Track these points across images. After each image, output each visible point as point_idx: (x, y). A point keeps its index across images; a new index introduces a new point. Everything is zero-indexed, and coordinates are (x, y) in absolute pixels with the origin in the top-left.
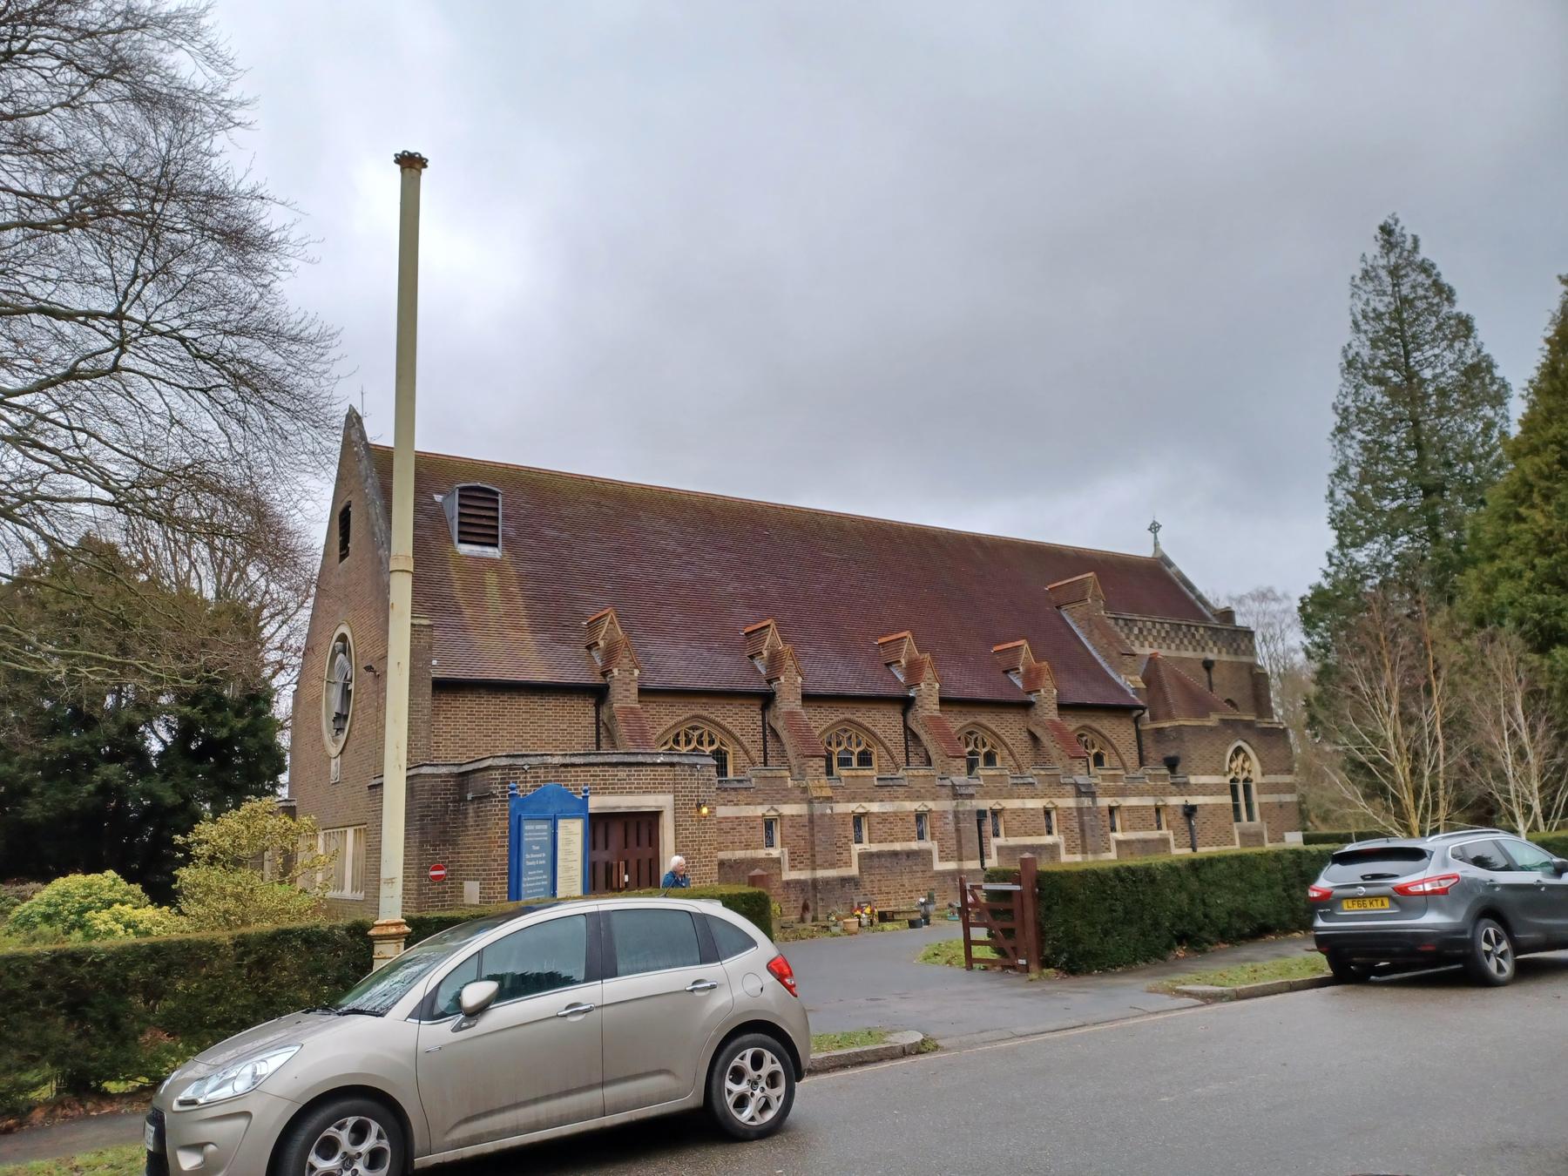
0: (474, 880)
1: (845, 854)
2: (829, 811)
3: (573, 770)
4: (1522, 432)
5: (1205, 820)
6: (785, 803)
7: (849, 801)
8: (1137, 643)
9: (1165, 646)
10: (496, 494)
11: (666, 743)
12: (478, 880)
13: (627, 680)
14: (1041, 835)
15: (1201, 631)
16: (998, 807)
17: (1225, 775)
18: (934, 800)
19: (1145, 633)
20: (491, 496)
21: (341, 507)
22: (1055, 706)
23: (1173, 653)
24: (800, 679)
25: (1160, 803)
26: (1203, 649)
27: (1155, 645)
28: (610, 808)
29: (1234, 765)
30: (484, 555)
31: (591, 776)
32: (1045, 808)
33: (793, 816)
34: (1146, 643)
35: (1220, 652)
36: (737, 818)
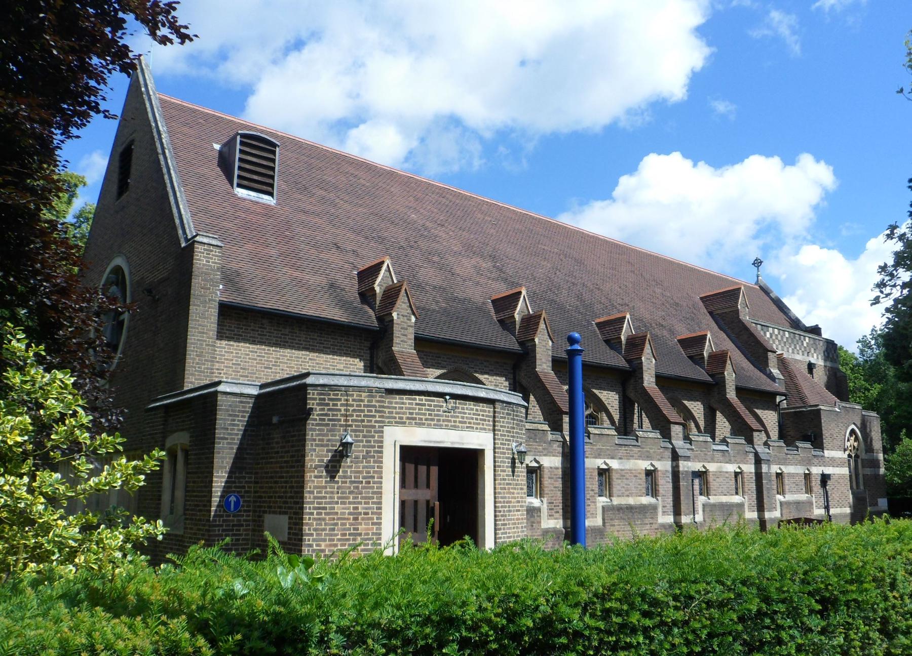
0: (280, 513)
3: (417, 397)
4: (191, 437)
5: (833, 487)
6: (545, 455)
10: (275, 145)
12: (285, 513)
15: (807, 339)
16: (605, 467)
17: (845, 450)
18: (659, 460)
21: (120, 149)
22: (734, 387)
24: (550, 343)
25: (807, 472)
28: (435, 442)
30: (260, 201)
31: (417, 404)
33: (551, 468)
35: (818, 358)
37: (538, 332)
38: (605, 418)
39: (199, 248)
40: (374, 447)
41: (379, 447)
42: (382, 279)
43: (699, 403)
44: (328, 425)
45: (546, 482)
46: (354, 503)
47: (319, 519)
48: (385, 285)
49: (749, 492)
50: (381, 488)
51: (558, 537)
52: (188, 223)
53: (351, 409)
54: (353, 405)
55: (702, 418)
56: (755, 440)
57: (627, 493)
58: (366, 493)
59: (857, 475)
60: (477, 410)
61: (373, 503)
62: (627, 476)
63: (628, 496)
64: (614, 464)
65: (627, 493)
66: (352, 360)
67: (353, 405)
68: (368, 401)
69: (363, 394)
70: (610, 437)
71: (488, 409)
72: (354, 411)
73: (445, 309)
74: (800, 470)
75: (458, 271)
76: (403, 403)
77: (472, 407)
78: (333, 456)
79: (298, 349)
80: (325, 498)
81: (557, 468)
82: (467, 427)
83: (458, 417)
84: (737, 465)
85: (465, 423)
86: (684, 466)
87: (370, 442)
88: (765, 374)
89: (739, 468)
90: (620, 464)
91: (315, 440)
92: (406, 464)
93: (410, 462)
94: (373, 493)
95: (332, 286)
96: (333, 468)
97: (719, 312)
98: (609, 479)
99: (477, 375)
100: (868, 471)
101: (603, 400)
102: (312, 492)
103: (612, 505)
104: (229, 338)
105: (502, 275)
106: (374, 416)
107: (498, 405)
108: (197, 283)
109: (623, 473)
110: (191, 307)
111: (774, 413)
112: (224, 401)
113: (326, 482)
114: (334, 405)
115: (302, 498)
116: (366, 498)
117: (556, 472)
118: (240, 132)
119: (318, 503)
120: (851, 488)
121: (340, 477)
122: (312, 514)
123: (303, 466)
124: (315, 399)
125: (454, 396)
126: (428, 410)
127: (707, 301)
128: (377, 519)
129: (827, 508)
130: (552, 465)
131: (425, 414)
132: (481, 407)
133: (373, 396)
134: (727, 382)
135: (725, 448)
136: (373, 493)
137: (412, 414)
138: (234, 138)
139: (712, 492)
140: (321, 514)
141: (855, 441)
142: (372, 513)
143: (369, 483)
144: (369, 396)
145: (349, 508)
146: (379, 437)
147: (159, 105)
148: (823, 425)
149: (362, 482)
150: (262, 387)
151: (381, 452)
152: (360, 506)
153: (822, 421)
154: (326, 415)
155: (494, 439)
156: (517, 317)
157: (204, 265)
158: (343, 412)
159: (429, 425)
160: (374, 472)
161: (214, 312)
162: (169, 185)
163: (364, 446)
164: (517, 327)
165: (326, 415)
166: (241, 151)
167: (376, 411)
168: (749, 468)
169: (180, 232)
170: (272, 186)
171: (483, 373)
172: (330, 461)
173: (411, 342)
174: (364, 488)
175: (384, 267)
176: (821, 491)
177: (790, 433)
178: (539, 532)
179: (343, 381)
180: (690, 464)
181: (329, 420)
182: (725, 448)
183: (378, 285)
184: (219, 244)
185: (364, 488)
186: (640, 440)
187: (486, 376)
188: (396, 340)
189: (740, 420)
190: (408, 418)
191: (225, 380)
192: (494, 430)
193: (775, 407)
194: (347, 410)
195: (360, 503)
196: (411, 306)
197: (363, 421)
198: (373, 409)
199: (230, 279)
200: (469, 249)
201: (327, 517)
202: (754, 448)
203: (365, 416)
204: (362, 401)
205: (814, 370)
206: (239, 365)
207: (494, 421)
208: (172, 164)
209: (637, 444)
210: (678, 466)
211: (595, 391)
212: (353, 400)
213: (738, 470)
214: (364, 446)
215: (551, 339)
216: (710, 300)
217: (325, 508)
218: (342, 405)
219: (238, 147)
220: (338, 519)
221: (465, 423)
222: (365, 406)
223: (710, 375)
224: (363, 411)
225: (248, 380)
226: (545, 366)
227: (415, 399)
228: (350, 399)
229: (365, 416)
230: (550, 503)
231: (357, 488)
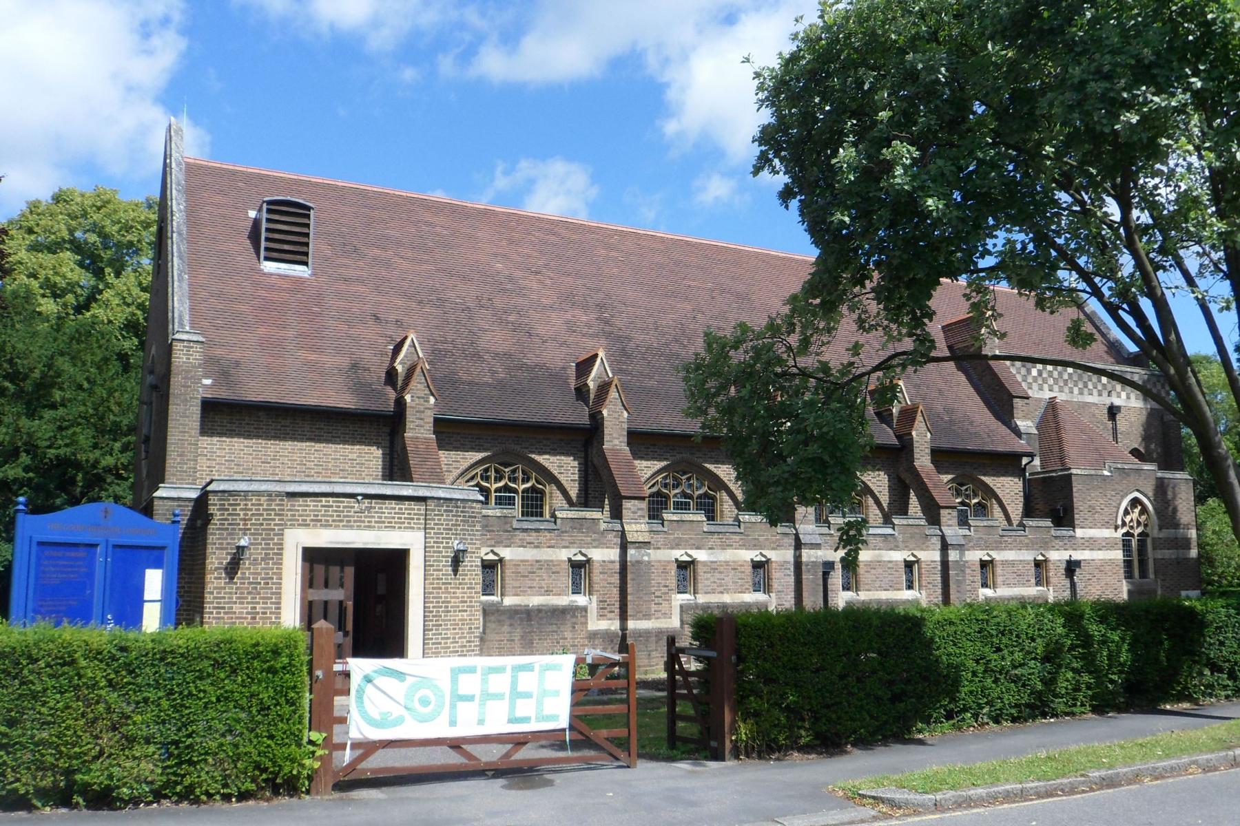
1: (665, 604)
2: (646, 558)
3: (324, 499)
5: (1088, 576)
6: (595, 547)
7: (673, 548)
8: (1035, 386)
9: (1066, 389)
10: (309, 208)
11: (472, 478)
13: (422, 408)
14: (899, 590)
16: (686, 558)
17: (1116, 528)
18: (773, 549)
19: (1045, 375)
20: (302, 210)
22: (928, 451)
23: (1076, 398)
24: (626, 414)
25: (1040, 558)
26: (1109, 394)
27: (1056, 388)
28: (343, 543)
29: (1128, 519)
30: (292, 273)
31: (322, 506)
32: (905, 561)
33: (604, 561)
34: (1046, 386)
35: (1128, 398)
36: (537, 561)
37: (607, 402)
38: (725, 497)
39: (177, 346)
40: (273, 549)
41: (278, 549)
42: (405, 356)
43: (882, 473)
44: (227, 529)
45: (597, 577)
46: (252, 603)
47: (219, 618)
48: (409, 363)
49: (930, 586)
50: (280, 588)
51: (612, 641)
52: (181, 317)
53: (250, 513)
54: (251, 510)
55: (886, 492)
56: (943, 520)
57: (721, 589)
58: (264, 593)
59: (1143, 563)
60: (401, 509)
61: (271, 603)
62: (722, 569)
63: (722, 593)
64: (701, 555)
65: (721, 589)
66: (366, 448)
67: (251, 510)
68: (268, 505)
69: (262, 498)
70: (695, 525)
71: (419, 508)
72: (253, 515)
73: (500, 381)
74: (1029, 556)
75: (540, 330)
76: (307, 506)
77: (393, 506)
78: (232, 559)
79: (302, 440)
80: (224, 598)
81: (613, 562)
82: (386, 527)
83: (374, 517)
84: (910, 553)
85: (384, 522)
86: (807, 555)
87: (269, 544)
88: (1009, 427)
89: (913, 555)
90: (709, 555)
91: (215, 544)
92: (316, 566)
93: (319, 563)
94: (272, 593)
95: (354, 366)
96: (232, 568)
97: (960, 345)
98: (694, 572)
99: (533, 456)
100: (1168, 554)
101: (722, 476)
102: (212, 593)
103: (696, 604)
104: (212, 435)
105: (607, 329)
106: (274, 520)
107: (429, 502)
108: (176, 382)
109: (713, 567)
110: (170, 407)
111: (1016, 480)
112: (160, 505)
113: (225, 583)
114: (233, 510)
115: (203, 598)
116: (264, 598)
117: (611, 566)
118: (266, 199)
119: (217, 603)
120: (1129, 575)
121: (238, 578)
122: (212, 613)
123: (204, 568)
124: (215, 505)
125: (366, 496)
126: (336, 511)
127: (949, 330)
128: (276, 618)
129: (623, 617)
130: (606, 559)
131: (333, 516)
132: (414, 506)
133: (272, 500)
134: (916, 445)
135: (890, 531)
136: (272, 593)
137: (317, 516)
138: (261, 207)
139: (862, 586)
140: (220, 613)
141: (1141, 513)
142: (271, 613)
143: (268, 583)
144: (268, 500)
145: (247, 608)
146: (278, 539)
147: (182, 177)
148: (1075, 494)
149: (260, 583)
150: (202, 489)
151: (281, 554)
152: (258, 606)
153: (1074, 490)
154: (226, 520)
155: (426, 538)
156: (591, 384)
157: (184, 362)
158: (242, 516)
159: (337, 527)
160: (273, 573)
161: (196, 411)
162: (170, 274)
163: (263, 549)
164: (592, 396)
165: (226, 520)
166: (268, 220)
167: (276, 515)
168: (930, 556)
169: (171, 327)
170: (307, 254)
171: (541, 453)
172: (229, 563)
173: (430, 426)
174: (263, 588)
175: (408, 342)
176: (1067, 583)
177: (1037, 507)
178: (583, 635)
179: (243, 487)
180: (819, 553)
181: (229, 524)
182: (890, 531)
183: (400, 363)
184: (201, 339)
185: (263, 588)
186: (742, 525)
187: (547, 457)
188: (409, 425)
189: (927, 494)
190: (312, 520)
191: (216, 477)
192: (425, 529)
193: (1020, 472)
194: (246, 515)
195: (259, 603)
196: (428, 387)
197: (262, 524)
198: (273, 513)
199: (223, 373)
200: (568, 299)
201: (226, 616)
202: (941, 530)
203: (264, 519)
204: (260, 505)
205: (1118, 417)
206: (233, 461)
207: (426, 520)
208: (179, 249)
209: (738, 530)
210: (800, 556)
211: (708, 466)
212: (252, 505)
213: (913, 559)
214: (263, 549)
215: (626, 409)
216: (952, 329)
217: (224, 608)
218: (241, 510)
219: (265, 215)
220: (237, 618)
221: (384, 522)
222: (264, 510)
223: (896, 436)
224: (262, 515)
225: (187, 484)
226: (616, 442)
227: (321, 501)
228: (249, 503)
229: (264, 519)
230: (601, 601)
231: (256, 588)
